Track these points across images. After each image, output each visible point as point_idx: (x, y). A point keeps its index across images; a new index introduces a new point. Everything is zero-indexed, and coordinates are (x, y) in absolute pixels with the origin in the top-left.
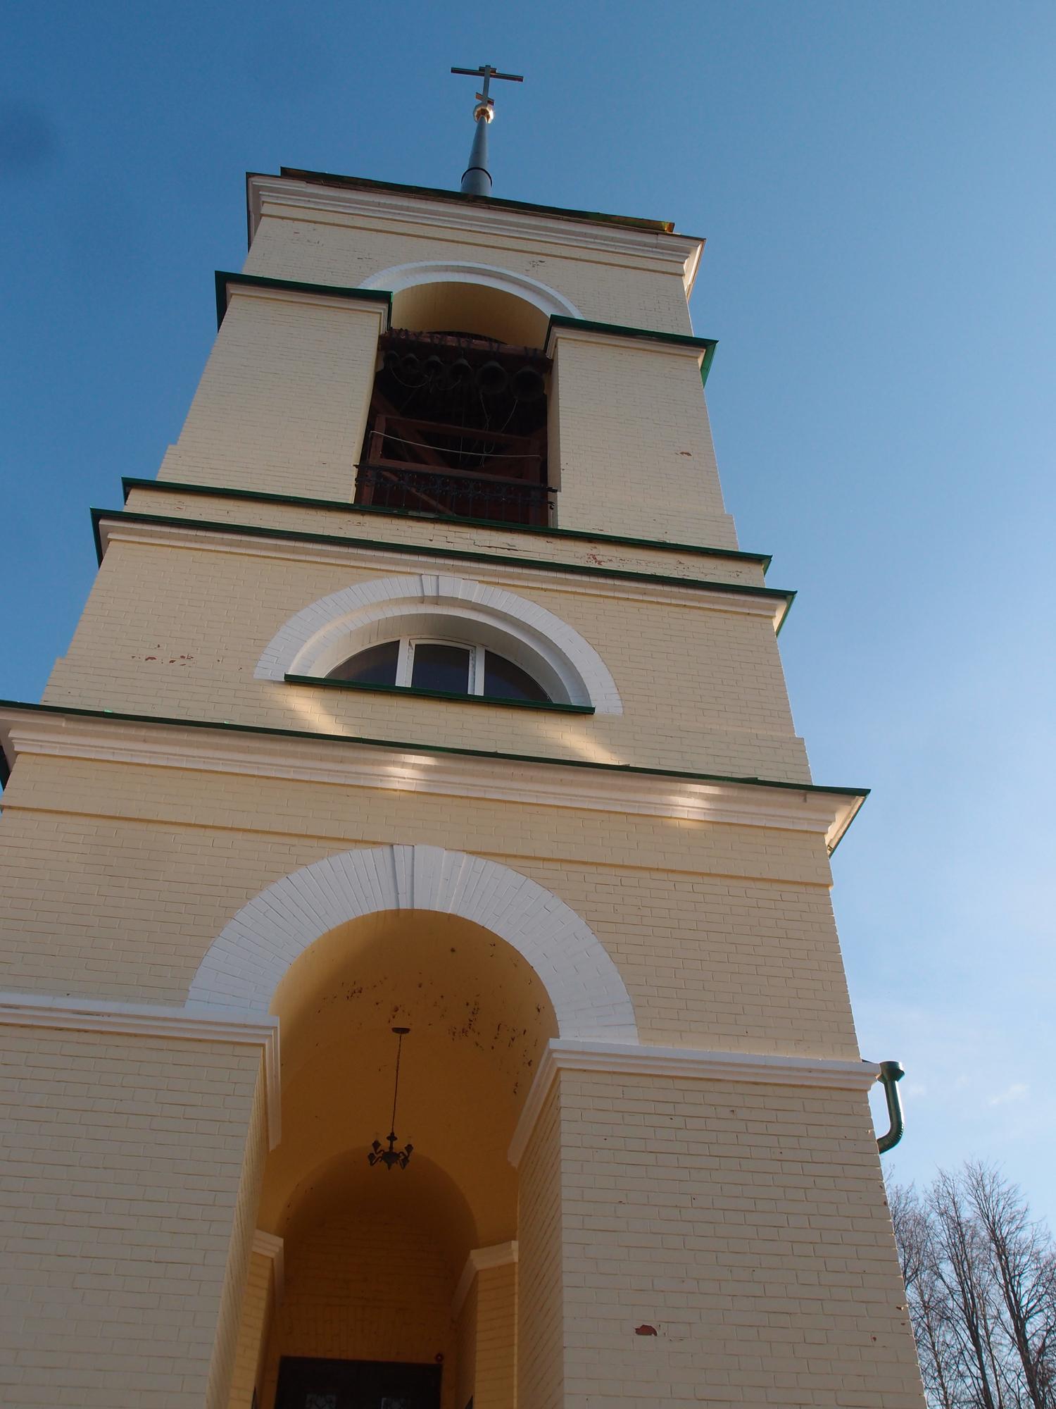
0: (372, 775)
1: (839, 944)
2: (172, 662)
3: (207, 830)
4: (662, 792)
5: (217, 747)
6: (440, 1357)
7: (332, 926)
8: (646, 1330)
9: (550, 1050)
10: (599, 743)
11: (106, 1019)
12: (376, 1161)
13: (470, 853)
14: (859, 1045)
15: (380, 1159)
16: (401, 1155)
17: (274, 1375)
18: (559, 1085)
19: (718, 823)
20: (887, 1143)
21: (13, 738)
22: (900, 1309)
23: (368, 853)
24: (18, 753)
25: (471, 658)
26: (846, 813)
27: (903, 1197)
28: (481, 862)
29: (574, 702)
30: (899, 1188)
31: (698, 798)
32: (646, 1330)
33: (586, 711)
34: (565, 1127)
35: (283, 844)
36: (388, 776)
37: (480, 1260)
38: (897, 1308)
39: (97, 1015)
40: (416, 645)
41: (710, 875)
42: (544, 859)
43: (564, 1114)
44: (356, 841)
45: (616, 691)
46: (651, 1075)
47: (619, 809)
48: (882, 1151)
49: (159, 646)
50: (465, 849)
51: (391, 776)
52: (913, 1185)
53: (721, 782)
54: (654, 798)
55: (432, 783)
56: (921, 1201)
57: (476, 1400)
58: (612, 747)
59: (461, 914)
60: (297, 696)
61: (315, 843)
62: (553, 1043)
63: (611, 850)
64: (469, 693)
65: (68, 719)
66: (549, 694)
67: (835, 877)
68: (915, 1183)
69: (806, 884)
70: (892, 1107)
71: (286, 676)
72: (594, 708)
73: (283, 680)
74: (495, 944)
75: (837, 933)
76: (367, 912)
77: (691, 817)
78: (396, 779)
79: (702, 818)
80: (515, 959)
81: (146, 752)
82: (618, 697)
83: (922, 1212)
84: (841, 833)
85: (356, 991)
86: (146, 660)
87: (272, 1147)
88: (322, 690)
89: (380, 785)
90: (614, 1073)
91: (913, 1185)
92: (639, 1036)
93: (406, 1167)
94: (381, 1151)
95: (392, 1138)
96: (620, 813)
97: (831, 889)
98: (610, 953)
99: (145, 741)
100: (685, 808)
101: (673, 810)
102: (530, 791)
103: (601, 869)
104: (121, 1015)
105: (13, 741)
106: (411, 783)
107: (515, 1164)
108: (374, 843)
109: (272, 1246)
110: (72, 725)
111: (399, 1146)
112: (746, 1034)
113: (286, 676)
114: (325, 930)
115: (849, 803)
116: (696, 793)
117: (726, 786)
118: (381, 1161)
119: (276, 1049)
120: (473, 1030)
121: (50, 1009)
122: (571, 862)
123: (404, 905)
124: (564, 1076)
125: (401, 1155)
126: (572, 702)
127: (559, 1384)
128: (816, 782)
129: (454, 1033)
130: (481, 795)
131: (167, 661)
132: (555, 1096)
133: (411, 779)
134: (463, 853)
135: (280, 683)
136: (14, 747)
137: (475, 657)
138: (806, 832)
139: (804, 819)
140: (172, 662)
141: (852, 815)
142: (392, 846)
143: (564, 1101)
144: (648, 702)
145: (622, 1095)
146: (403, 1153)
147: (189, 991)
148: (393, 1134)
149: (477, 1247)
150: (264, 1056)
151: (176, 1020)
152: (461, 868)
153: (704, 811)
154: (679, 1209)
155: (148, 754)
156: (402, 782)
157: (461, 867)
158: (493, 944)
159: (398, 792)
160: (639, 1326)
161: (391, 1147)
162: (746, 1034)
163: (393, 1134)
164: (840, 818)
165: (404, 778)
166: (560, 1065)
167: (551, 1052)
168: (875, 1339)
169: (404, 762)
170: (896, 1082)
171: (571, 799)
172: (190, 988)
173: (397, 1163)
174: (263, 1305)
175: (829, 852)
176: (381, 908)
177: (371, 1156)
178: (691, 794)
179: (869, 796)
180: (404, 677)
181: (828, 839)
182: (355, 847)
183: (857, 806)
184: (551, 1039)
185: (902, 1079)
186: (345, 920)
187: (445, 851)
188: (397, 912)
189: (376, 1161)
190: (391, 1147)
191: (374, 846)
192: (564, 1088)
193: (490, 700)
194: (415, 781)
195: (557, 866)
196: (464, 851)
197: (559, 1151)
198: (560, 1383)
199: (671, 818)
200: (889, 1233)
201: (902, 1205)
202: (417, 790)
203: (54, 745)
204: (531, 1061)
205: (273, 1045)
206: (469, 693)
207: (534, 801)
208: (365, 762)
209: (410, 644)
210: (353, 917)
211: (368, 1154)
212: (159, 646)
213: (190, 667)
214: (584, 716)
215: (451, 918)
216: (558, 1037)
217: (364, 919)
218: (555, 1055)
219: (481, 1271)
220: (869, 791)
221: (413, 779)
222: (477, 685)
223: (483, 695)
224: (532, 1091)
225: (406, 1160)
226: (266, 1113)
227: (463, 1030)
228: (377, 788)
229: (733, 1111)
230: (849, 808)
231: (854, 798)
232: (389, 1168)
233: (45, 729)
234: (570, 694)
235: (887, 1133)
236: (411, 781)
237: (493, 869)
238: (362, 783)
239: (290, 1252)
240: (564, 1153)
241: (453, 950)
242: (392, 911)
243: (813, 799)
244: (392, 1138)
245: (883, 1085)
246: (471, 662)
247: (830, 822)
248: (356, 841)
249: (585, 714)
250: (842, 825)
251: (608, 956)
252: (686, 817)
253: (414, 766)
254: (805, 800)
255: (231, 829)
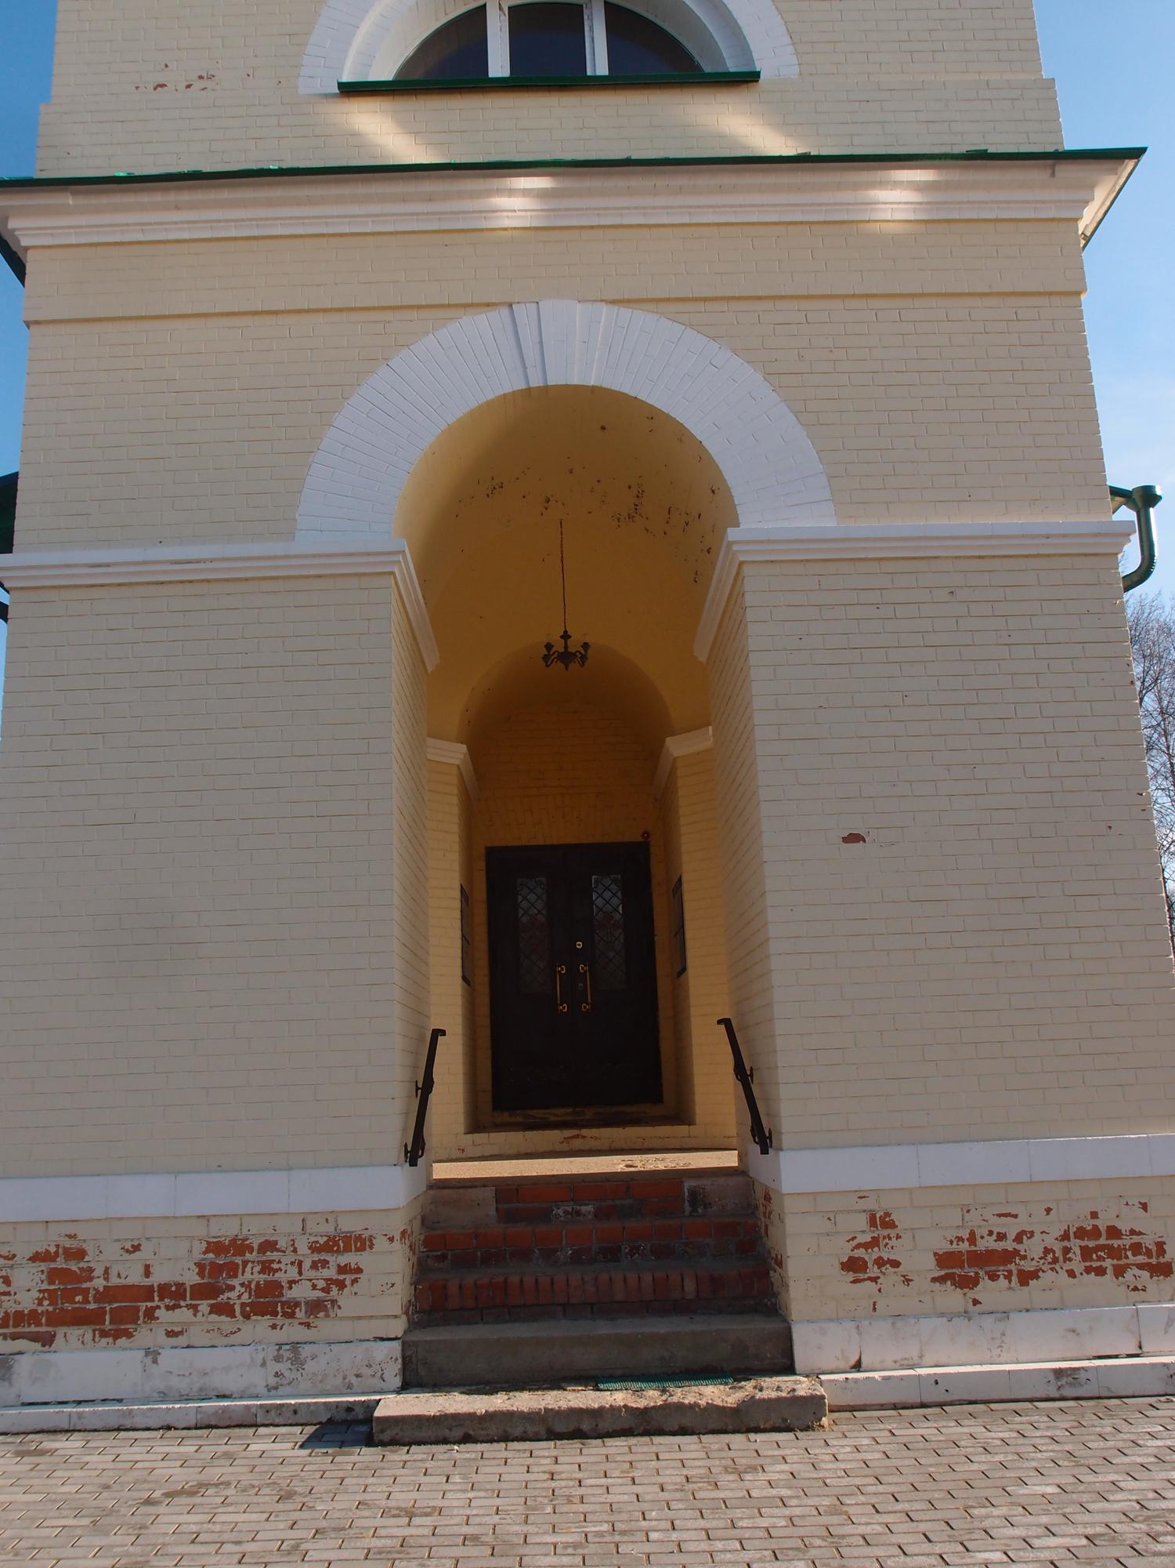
0: (474, 212)
1: (1082, 307)
2: (189, 86)
3: (279, 316)
4: (856, 187)
5: (270, 203)
6: (646, 834)
7: (451, 420)
8: (854, 838)
9: (729, 542)
10: (769, 124)
11: (209, 565)
12: (552, 663)
13: (611, 302)
14: (1098, 409)
15: (555, 660)
16: (577, 654)
17: (482, 864)
18: (743, 580)
19: (933, 221)
20: (1136, 579)
21: (14, 230)
22: (1141, 795)
23: (482, 321)
24: (27, 249)
25: (585, 17)
26: (1111, 184)
27: (1147, 607)
28: (625, 313)
29: (732, 66)
30: (1143, 597)
31: (906, 189)
32: (854, 838)
33: (748, 78)
34: (752, 629)
35: (376, 322)
36: (493, 211)
37: (677, 747)
38: (1139, 794)
39: (197, 562)
40: (509, 8)
41: (922, 295)
42: (705, 299)
43: (750, 615)
44: (465, 306)
45: (787, 40)
46: (852, 559)
47: (799, 218)
48: (1127, 589)
49: (166, 66)
50: (603, 298)
51: (496, 211)
52: (1160, 593)
53: (936, 162)
54: (847, 196)
55: (552, 213)
56: (1168, 609)
57: (684, 879)
58: (784, 125)
59: (607, 384)
60: (359, 112)
61: (414, 314)
62: (732, 534)
63: (792, 275)
64: (589, 73)
65: (74, 193)
66: (697, 58)
67: (1089, 280)
68: (1162, 592)
69: (1050, 294)
70: (1144, 539)
71: (341, 85)
72: (759, 72)
73: (338, 91)
74: (653, 419)
75: (1090, 357)
76: (491, 396)
77: (897, 216)
78: (505, 214)
79: (912, 217)
80: (681, 434)
81: (182, 222)
82: (791, 49)
83: (1168, 620)
84: (1100, 215)
85: (497, 487)
86: (155, 89)
87: (430, 669)
88: (391, 98)
89: (484, 224)
90: (807, 561)
91: (1160, 593)
92: (836, 515)
93: (586, 664)
94: (555, 652)
95: (566, 636)
96: (801, 223)
97: (1083, 297)
98: (796, 414)
99: (177, 208)
100: (888, 206)
101: (872, 210)
102: (680, 207)
103: (780, 304)
104: (223, 559)
105: (16, 233)
106: (524, 216)
107: (703, 658)
108: (488, 305)
109: (456, 754)
110: (83, 201)
111: (574, 646)
112: (969, 499)
113: (341, 85)
114: (444, 426)
115: (1114, 171)
116: (903, 181)
117: (947, 167)
118: (556, 662)
119: (409, 573)
120: (640, 515)
121: (145, 563)
122: (739, 298)
123: (536, 382)
124: (747, 570)
125: (577, 654)
126: (728, 66)
127: (762, 895)
128: (1070, 144)
129: (619, 520)
130: (617, 221)
131: (182, 86)
132: (738, 595)
133: (522, 211)
134: (600, 304)
135: (334, 96)
136: (19, 241)
137: (592, 13)
138: (1053, 220)
139: (1050, 202)
140: (189, 86)
141: (1118, 188)
142: (510, 305)
143: (749, 600)
144: (835, 52)
145: (818, 586)
146: (580, 652)
147: (296, 520)
148: (566, 632)
149: (673, 734)
150: (396, 583)
151: (287, 557)
152: (602, 324)
153: (913, 206)
154: (888, 709)
155: (186, 226)
156: (512, 217)
157: (600, 322)
158: (650, 417)
159: (510, 232)
160: (846, 834)
161: (566, 647)
162: (969, 499)
163: (566, 632)
164: (1101, 195)
165: (515, 211)
166: (742, 559)
167: (731, 544)
168: (1110, 827)
169: (511, 189)
170: (1151, 509)
171: (735, 211)
172: (297, 517)
173: (575, 662)
174: (456, 810)
175: (1083, 242)
176: (508, 389)
177: (545, 658)
178: (896, 185)
179: (1144, 158)
180: (499, 64)
181: (1081, 226)
182: (465, 315)
183: (1125, 174)
184: (729, 529)
185: (1159, 504)
186: (466, 409)
187: (579, 305)
188: (528, 391)
189: (552, 663)
190: (566, 647)
191: (489, 308)
192: (748, 585)
193: (620, 80)
194: (528, 214)
195: (723, 306)
196: (602, 301)
197: (748, 656)
198: (763, 894)
199: (868, 221)
200: (1136, 715)
201: (1146, 615)
202: (532, 225)
203: (67, 231)
204: (710, 548)
205: (406, 569)
206: (589, 73)
207: (686, 220)
208: (461, 195)
209: (501, 8)
210: (474, 404)
211: (542, 656)
212: (166, 66)
213: (213, 90)
214: (746, 86)
215: (594, 390)
216: (737, 525)
217: (489, 405)
218: (735, 548)
219: (678, 757)
220: (1143, 150)
221: (525, 211)
222: (598, 62)
223: (607, 74)
224: (715, 577)
225: (584, 658)
226: (415, 638)
227: (629, 515)
228: (482, 230)
229: (952, 592)
230: (1113, 178)
231: (1124, 162)
232: (567, 669)
233: (47, 211)
234: (725, 55)
235: (1138, 566)
236: (524, 214)
237: (642, 319)
238: (460, 225)
239: (474, 754)
240: (754, 659)
241: (603, 428)
242: (521, 391)
243: (1066, 171)
244: (566, 636)
245: (1135, 513)
246: (586, 23)
247: (1087, 202)
248: (465, 306)
249: (747, 82)
250: (1103, 203)
251: (794, 417)
252: (889, 218)
253: (526, 192)
254: (1053, 174)
255: (308, 311)
